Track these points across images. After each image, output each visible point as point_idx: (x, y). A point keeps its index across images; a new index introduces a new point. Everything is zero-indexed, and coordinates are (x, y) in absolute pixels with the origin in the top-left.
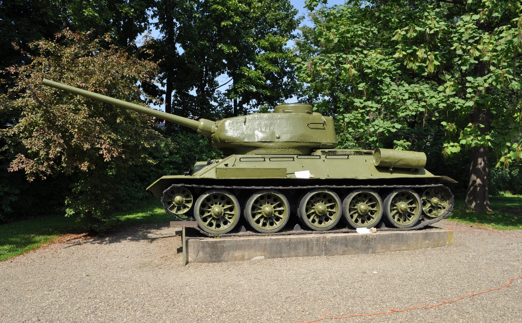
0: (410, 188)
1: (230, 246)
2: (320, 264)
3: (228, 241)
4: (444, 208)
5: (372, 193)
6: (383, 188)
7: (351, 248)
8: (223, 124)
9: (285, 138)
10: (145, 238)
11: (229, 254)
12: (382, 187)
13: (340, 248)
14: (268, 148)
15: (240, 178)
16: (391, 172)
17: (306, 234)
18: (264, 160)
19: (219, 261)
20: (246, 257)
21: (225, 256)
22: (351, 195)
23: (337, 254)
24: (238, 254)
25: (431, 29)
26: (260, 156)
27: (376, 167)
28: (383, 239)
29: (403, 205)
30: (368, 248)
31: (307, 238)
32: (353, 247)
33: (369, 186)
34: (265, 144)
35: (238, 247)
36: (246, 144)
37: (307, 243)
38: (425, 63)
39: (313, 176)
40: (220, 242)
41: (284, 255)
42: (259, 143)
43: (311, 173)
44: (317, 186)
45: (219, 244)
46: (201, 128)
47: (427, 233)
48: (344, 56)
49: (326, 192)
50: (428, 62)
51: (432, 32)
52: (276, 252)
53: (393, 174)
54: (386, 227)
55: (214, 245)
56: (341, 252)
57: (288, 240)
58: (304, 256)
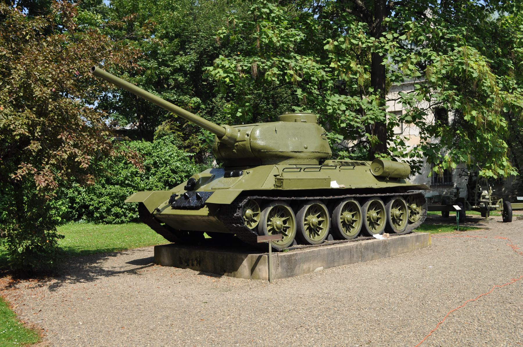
0: (320, 200)
1: (301, 259)
2: (373, 269)
3: (299, 253)
4: (418, 213)
5: (380, 201)
6: (386, 195)
7: (376, 253)
8: (253, 131)
9: (311, 149)
10: (102, 272)
11: (299, 267)
12: (328, 198)
13: (370, 254)
14: (300, 158)
15: (300, 189)
16: (387, 182)
17: (303, 248)
18: (300, 171)
19: (292, 276)
20: (311, 269)
21: (297, 270)
22: (304, 209)
23: (368, 260)
24: (305, 266)
25: (363, 43)
26: (295, 166)
27: (376, 177)
28: (395, 242)
29: (278, 221)
30: (386, 252)
31: (350, 246)
32: (377, 252)
33: (379, 195)
34: (298, 154)
35: (307, 259)
36: (281, 154)
37: (349, 250)
38: (356, 76)
39: (342, 186)
40: (293, 255)
41: (336, 265)
42: (294, 153)
43: (338, 183)
44: (349, 196)
45: (293, 258)
46: (229, 135)
47: (418, 236)
48: (286, 60)
49: (353, 201)
50: (358, 75)
51: (364, 46)
52: (331, 261)
53: (388, 183)
54: (335, 239)
55: (289, 259)
56: (370, 257)
57: (338, 249)
58: (348, 264)
